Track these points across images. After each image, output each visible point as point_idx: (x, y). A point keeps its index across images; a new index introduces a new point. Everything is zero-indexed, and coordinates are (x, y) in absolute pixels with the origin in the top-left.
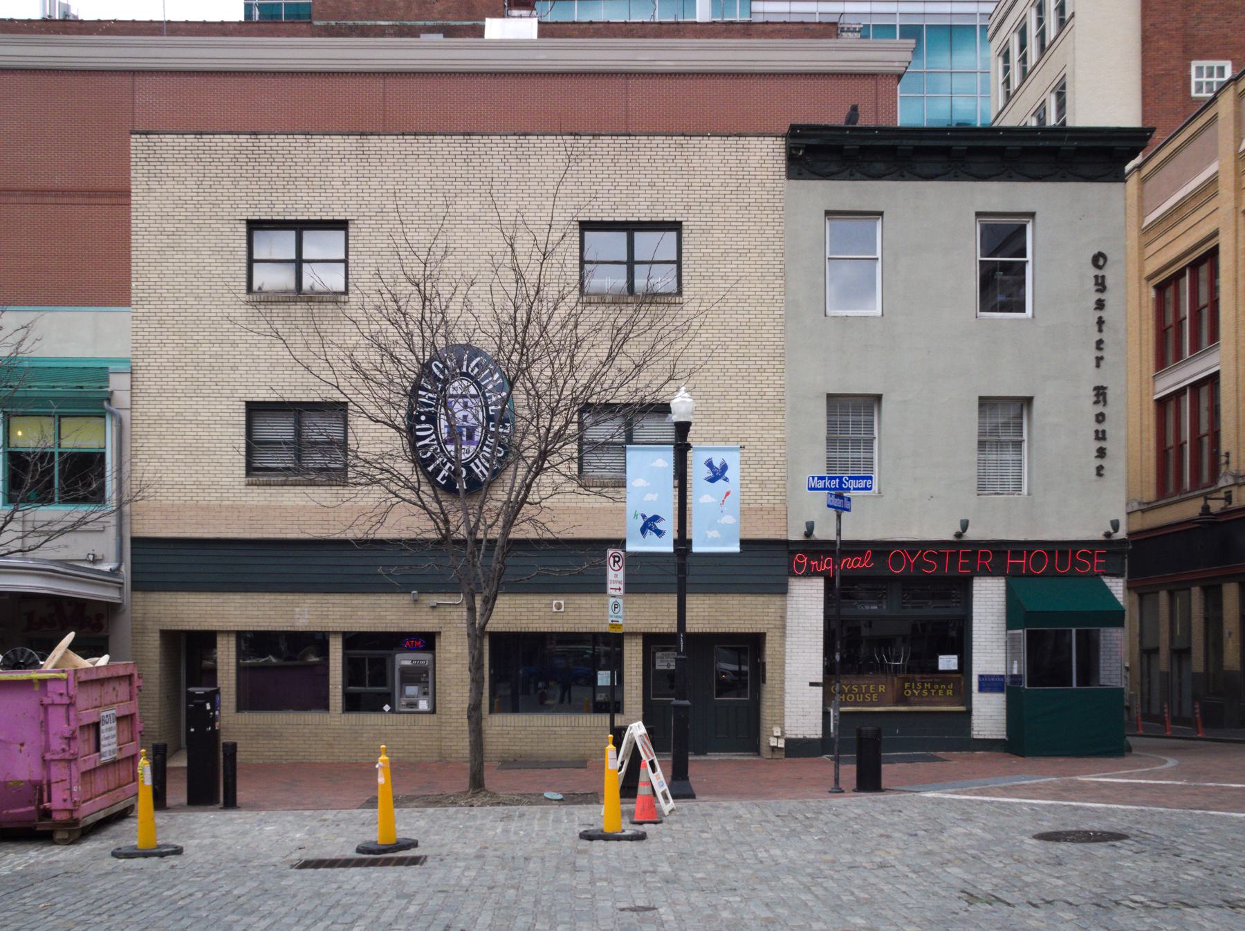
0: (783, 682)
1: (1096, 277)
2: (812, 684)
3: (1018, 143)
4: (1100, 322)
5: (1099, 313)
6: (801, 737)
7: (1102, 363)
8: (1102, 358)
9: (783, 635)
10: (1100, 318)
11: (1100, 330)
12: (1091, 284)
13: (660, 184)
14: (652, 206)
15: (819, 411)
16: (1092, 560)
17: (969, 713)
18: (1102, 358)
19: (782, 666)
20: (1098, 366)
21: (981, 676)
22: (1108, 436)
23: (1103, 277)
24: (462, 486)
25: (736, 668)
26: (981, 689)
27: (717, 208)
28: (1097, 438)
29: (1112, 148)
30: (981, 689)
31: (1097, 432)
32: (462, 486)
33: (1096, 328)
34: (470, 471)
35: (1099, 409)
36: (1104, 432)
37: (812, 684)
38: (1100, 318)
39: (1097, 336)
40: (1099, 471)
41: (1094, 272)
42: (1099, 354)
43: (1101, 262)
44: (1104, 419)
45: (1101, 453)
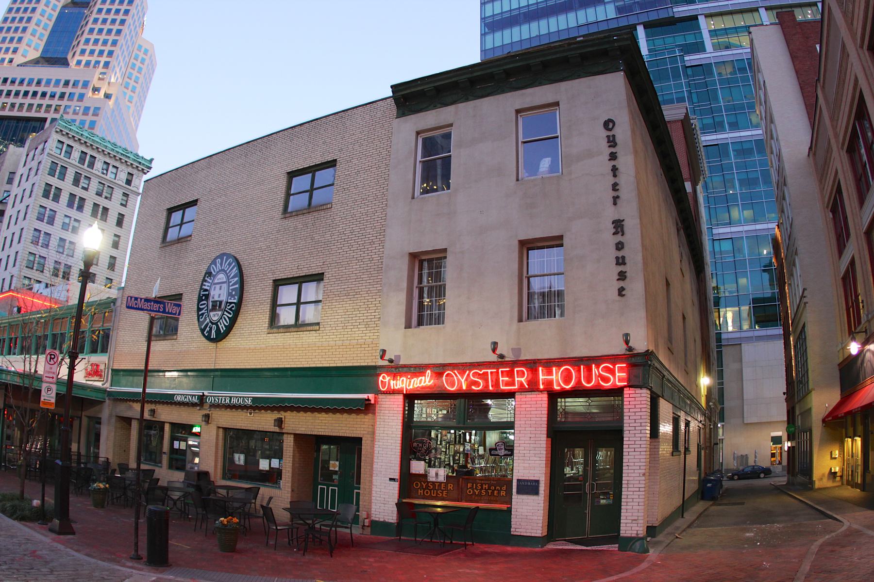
0: (372, 476)
1: (608, 137)
2: (391, 479)
3: (579, 52)
4: (614, 169)
5: (613, 163)
6: (382, 520)
7: (618, 201)
8: (618, 197)
9: (373, 440)
10: (614, 166)
11: (615, 176)
12: (604, 143)
13: (328, 140)
14: (194, 324)
15: (406, 259)
16: (613, 374)
17: (509, 511)
18: (618, 197)
19: (372, 464)
20: (615, 204)
21: (518, 480)
22: (627, 261)
23: (614, 136)
24: (213, 335)
25: (339, 529)
26: (519, 492)
27: (356, 147)
28: (618, 264)
29: (456, 82)
30: (518, 492)
31: (617, 258)
32: (213, 335)
33: (611, 174)
34: (218, 326)
35: (619, 238)
36: (623, 258)
37: (391, 479)
38: (614, 166)
39: (617, 180)
40: (621, 292)
41: (606, 133)
42: (615, 194)
43: (611, 126)
44: (623, 248)
45: (622, 276)
